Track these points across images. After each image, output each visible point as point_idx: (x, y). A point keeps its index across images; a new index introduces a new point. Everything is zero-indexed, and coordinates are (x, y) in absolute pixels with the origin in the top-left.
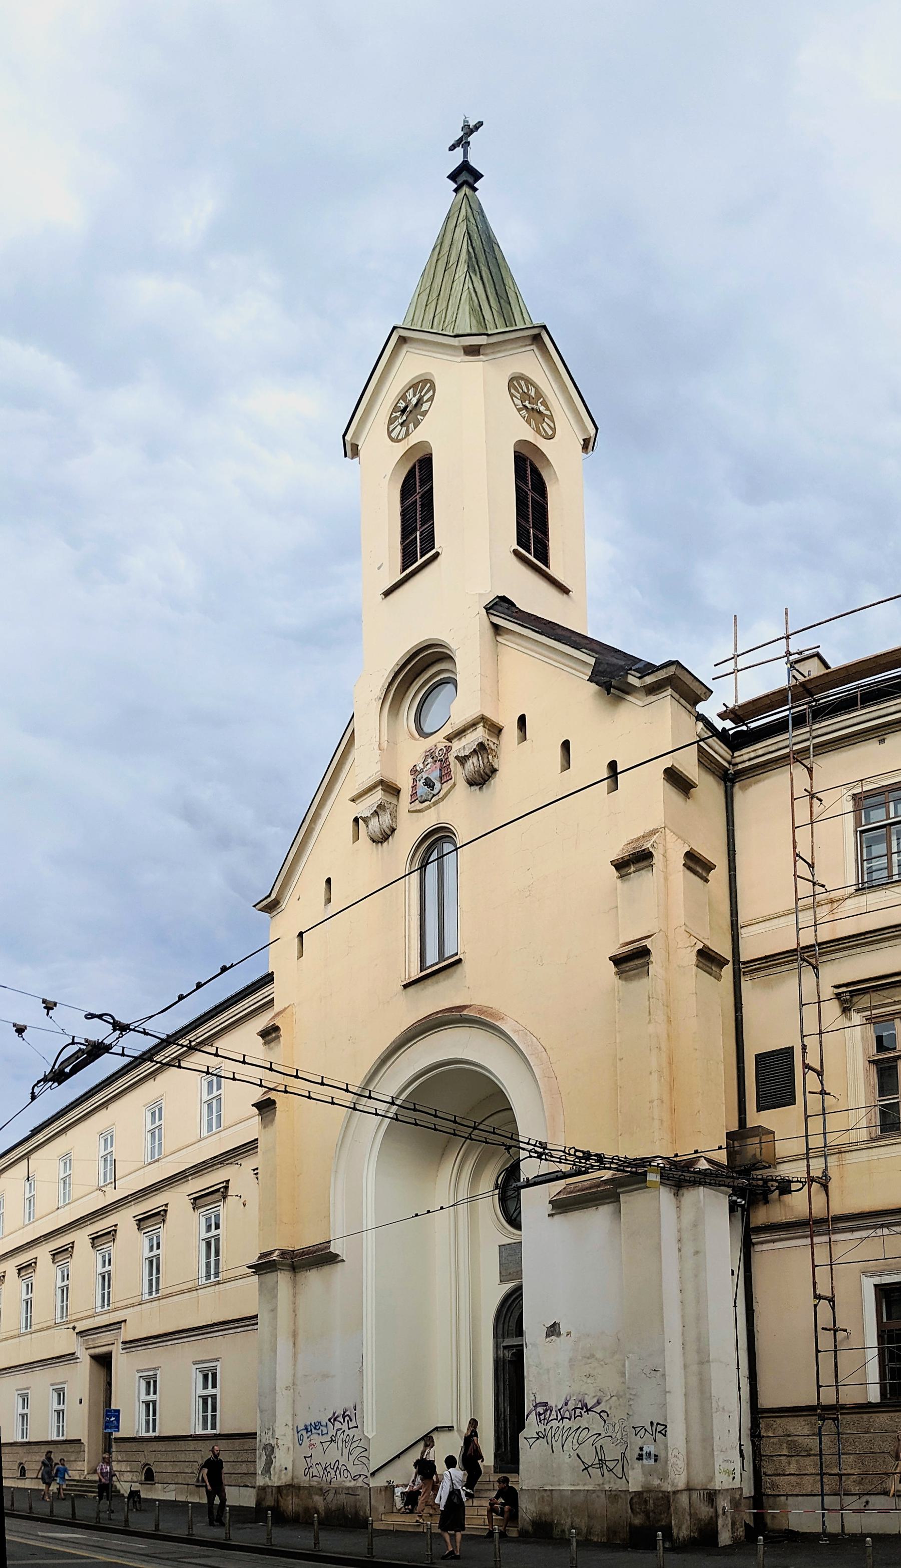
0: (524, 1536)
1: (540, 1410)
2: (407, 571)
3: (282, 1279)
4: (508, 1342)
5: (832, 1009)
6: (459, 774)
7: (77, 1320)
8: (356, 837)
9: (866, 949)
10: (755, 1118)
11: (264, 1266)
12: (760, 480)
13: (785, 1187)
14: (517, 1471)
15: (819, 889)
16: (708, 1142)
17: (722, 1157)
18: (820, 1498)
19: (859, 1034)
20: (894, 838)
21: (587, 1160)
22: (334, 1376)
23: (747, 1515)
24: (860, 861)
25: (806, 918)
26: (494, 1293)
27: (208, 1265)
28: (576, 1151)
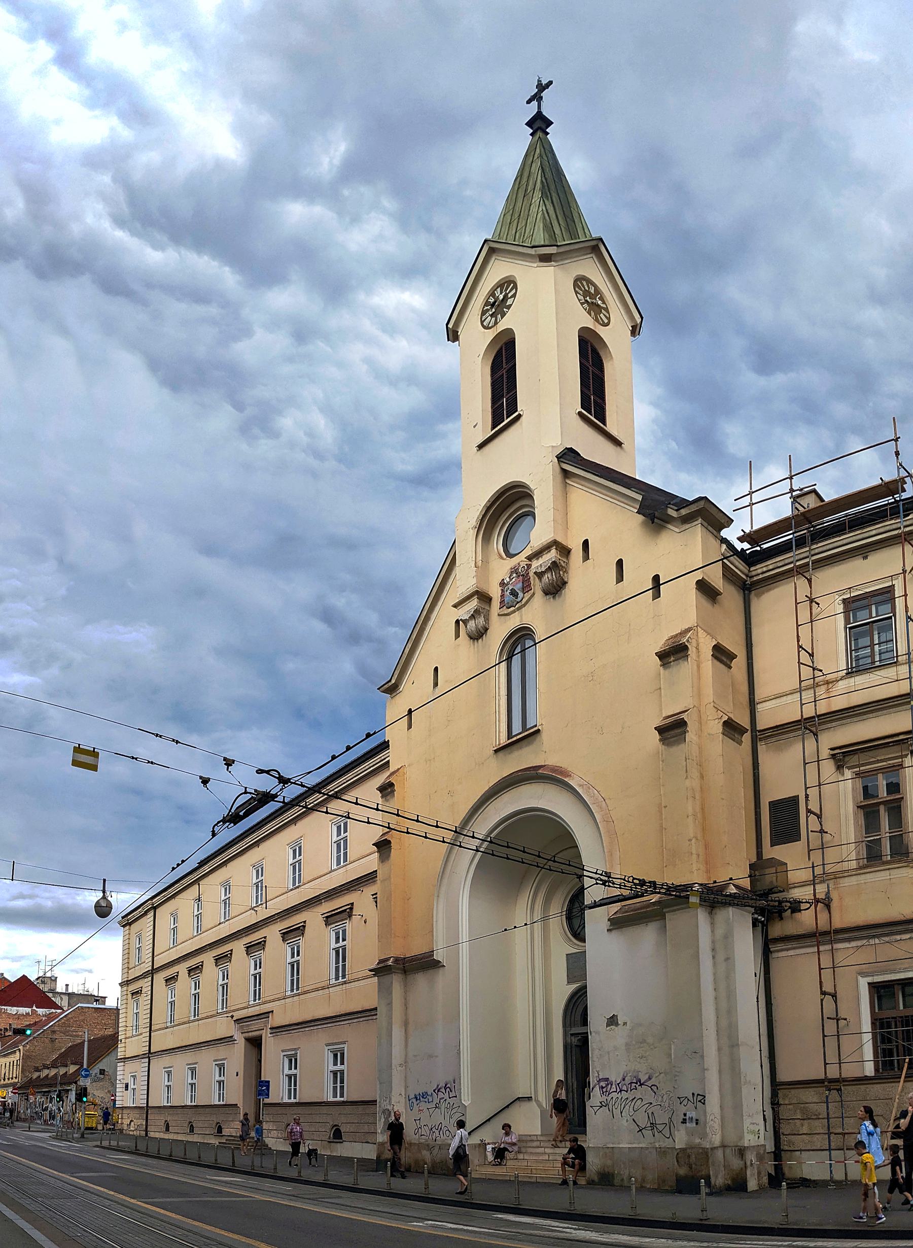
0: (591, 1183)
1: (603, 1084)
2: (496, 429)
3: (396, 981)
4: (575, 1030)
5: (828, 767)
6: (537, 586)
7: (234, 1011)
8: (457, 635)
9: (855, 719)
10: (770, 852)
11: (382, 970)
12: (768, 355)
13: (796, 906)
14: (585, 1133)
15: (818, 673)
16: (735, 872)
17: (746, 883)
18: (827, 1152)
19: (850, 785)
20: (876, 633)
21: (643, 886)
22: (437, 1057)
23: (769, 1166)
24: (849, 651)
25: (808, 696)
26: (562, 991)
27: (337, 969)
28: (634, 879)
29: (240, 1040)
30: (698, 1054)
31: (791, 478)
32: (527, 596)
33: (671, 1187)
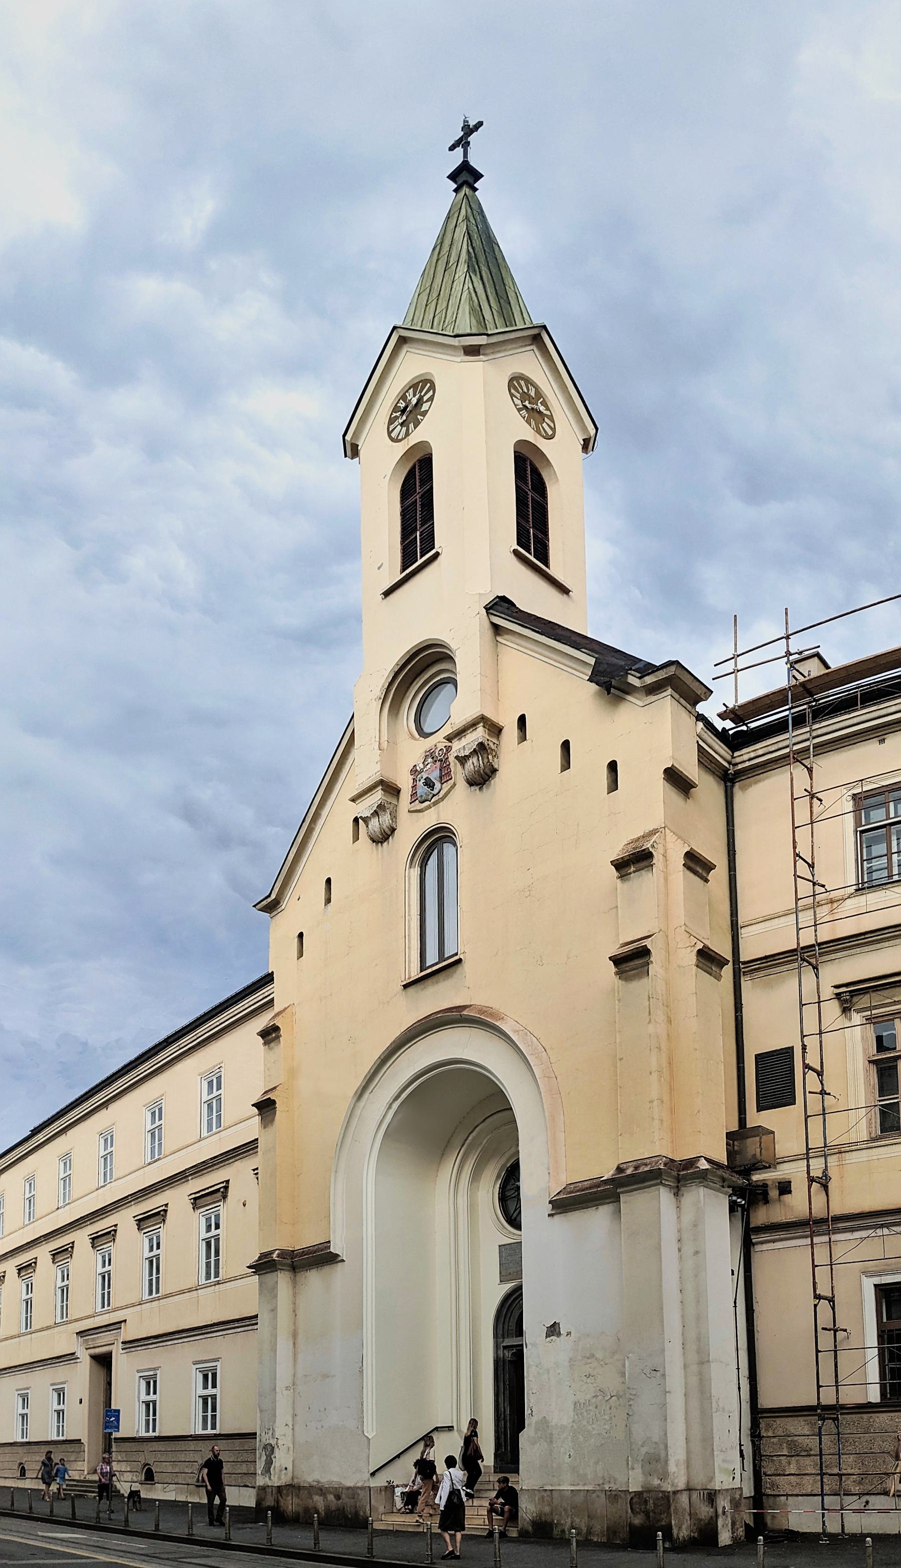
0: (524, 1536)
2: (407, 571)
3: (282, 1279)
4: (508, 1342)
5: (832, 1009)
6: (459, 774)
8: (356, 838)
9: (866, 949)
10: (755, 1119)
11: (264, 1265)
12: (760, 480)
14: (517, 1471)
15: (818, 889)
17: (723, 1158)
18: (820, 1498)
20: (894, 838)
22: (334, 1376)
23: (747, 1515)
24: (860, 861)
26: (494, 1293)
27: (208, 1265)
29: (85, 1363)
30: (657, 1371)
31: (788, 637)
32: (446, 786)
33: (624, 1540)
